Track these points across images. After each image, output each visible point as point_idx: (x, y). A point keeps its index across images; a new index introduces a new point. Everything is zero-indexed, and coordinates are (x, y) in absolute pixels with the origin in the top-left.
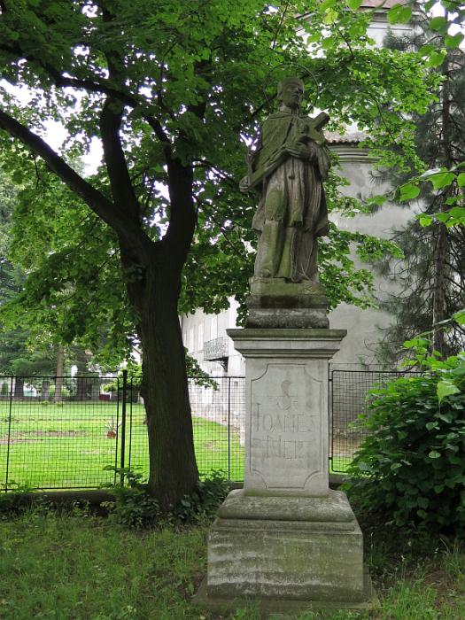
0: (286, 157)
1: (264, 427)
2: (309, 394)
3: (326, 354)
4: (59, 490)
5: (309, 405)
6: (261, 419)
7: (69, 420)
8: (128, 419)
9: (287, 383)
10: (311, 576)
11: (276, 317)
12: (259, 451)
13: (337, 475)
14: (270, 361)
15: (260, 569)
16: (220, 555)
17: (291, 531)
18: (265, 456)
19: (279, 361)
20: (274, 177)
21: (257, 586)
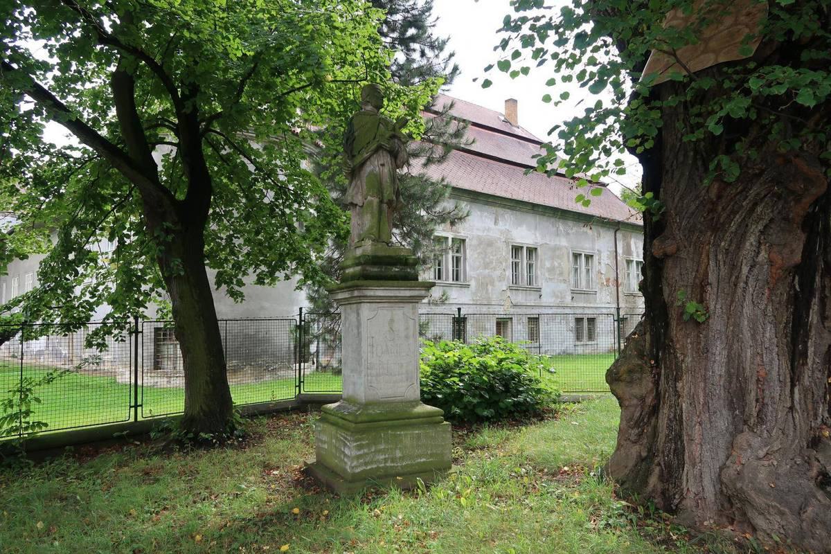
0: (380, 148)
1: (377, 355)
2: (407, 329)
3: (415, 300)
4: (74, 429)
5: (407, 337)
6: (374, 349)
7: (22, 359)
8: (133, 355)
9: (392, 321)
10: (420, 456)
11: (381, 271)
12: (374, 372)
13: (76, 431)
14: (380, 305)
15: (387, 456)
16: (359, 450)
17: (594, 395)
18: (378, 375)
19: (386, 305)
20: (368, 163)
21: (386, 468)
